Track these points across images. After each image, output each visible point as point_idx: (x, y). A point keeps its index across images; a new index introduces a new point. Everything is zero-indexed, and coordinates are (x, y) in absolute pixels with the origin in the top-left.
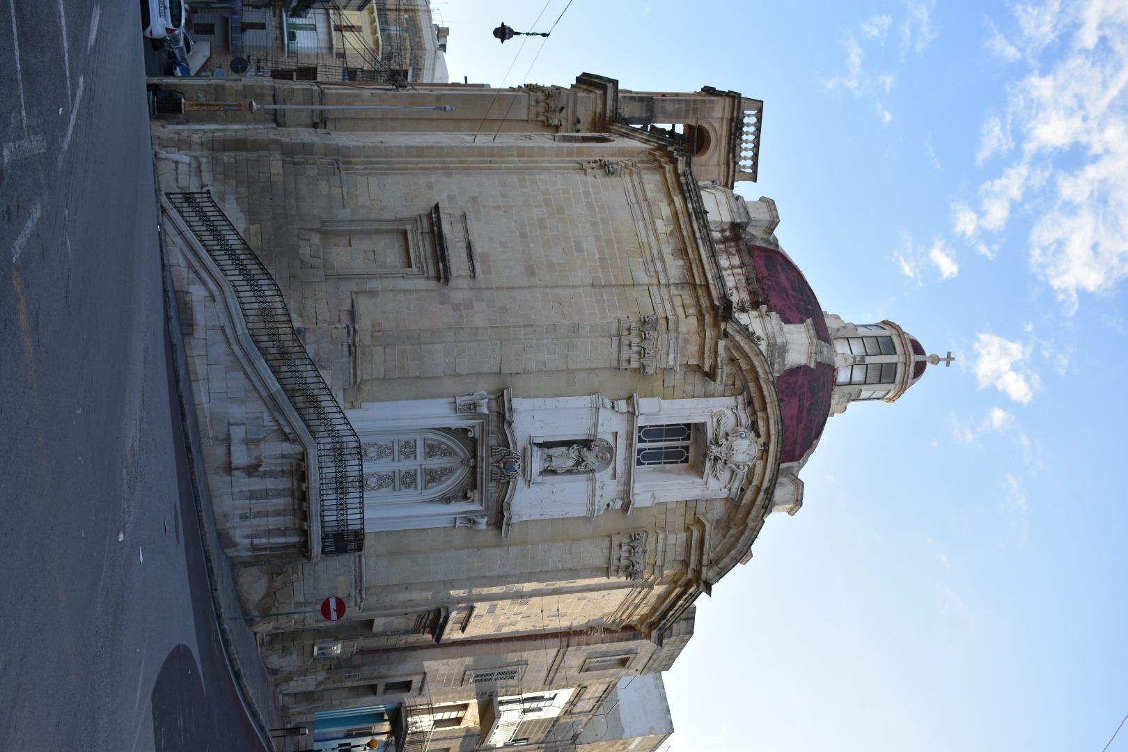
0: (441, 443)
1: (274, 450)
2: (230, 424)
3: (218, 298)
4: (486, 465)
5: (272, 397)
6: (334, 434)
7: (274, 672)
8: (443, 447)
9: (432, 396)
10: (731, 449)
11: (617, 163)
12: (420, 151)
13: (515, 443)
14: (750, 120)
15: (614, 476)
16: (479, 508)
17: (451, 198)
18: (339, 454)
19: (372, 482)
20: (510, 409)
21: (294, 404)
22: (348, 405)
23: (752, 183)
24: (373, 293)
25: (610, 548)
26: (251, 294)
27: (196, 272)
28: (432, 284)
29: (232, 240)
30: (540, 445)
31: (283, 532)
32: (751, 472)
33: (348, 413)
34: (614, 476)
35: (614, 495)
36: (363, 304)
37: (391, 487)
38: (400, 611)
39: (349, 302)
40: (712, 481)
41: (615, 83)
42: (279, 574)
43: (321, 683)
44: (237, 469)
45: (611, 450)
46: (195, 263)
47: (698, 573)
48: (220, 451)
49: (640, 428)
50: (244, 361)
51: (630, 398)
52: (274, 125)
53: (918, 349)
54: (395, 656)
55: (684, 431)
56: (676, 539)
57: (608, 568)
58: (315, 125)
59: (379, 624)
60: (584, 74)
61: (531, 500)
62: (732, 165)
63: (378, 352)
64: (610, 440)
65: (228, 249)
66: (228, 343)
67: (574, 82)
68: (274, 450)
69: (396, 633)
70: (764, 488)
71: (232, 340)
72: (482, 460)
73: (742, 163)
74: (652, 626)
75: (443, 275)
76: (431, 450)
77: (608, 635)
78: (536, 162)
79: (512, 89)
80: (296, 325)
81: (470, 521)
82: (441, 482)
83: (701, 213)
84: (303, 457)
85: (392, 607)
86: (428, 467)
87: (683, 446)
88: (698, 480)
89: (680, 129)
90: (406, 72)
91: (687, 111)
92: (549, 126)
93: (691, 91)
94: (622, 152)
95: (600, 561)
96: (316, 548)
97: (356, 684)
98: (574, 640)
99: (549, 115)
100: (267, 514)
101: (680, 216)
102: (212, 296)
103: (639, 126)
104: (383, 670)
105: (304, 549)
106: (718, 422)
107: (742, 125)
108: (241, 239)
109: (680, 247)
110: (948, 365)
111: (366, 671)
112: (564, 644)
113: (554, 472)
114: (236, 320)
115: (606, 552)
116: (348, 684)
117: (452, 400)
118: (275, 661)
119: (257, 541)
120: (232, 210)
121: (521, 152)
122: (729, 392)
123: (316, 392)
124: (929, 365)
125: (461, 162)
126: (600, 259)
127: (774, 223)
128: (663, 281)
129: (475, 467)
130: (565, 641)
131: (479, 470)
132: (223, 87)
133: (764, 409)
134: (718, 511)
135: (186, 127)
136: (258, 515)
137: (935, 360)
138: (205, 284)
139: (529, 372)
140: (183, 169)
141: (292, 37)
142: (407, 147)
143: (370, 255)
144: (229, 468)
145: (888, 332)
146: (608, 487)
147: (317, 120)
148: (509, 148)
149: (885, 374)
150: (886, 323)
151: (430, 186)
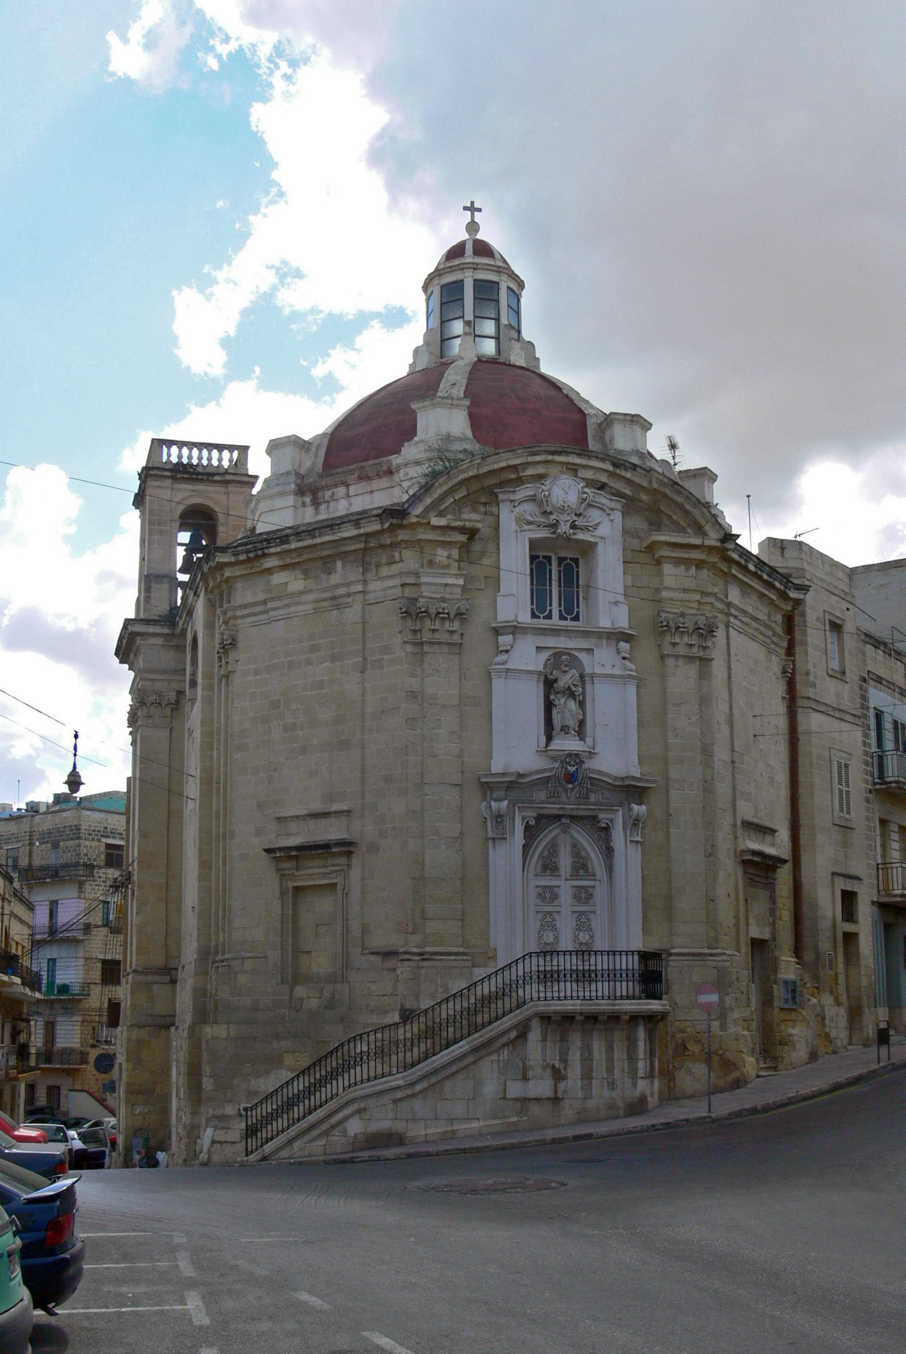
0: (541, 854)
1: (536, 1048)
2: (504, 1098)
3: (362, 1105)
4: (568, 804)
5: (475, 1050)
6: (526, 980)
7: (813, 1056)
8: (545, 853)
9: (486, 865)
10: (562, 509)
11: (222, 634)
12: (205, 865)
13: (544, 770)
14: (173, 455)
15: (590, 651)
16: (620, 813)
17: (258, 833)
18: (546, 977)
19: (584, 937)
20: (503, 774)
21: (484, 1026)
22: (492, 964)
23: (250, 452)
24: (365, 930)
25: (677, 657)
26: (358, 1069)
27: (333, 1127)
28: (356, 861)
29: (300, 1085)
30: (549, 738)
31: (632, 1043)
32: (590, 483)
33: (501, 964)
34: (590, 651)
35: (613, 651)
36: (377, 941)
37: (592, 917)
38: (742, 909)
39: (373, 958)
40: (600, 532)
41: (128, 622)
42: (685, 1048)
43: (838, 1003)
44: (556, 1092)
45: (558, 655)
46: (324, 1127)
47: (711, 549)
48: (535, 1110)
49: (534, 616)
50: (433, 1080)
51: (497, 632)
52: (173, 1029)
53: (456, 252)
54: (805, 909)
55: (539, 565)
56: (672, 575)
57: (701, 659)
58: (173, 982)
59: (756, 932)
60: (117, 654)
61: (614, 754)
62: (228, 477)
63: (431, 927)
64: (545, 655)
65: (309, 1091)
66: (413, 1096)
67: (126, 666)
68: (536, 1048)
69: (772, 912)
70: (611, 468)
71: (409, 1092)
72: (567, 807)
73: (226, 464)
74: (784, 596)
75: (347, 848)
76: (549, 867)
77: (798, 649)
78: (219, 728)
79: (134, 743)
80: (396, 1018)
81: (635, 825)
82: (587, 857)
83: (280, 537)
84: (546, 1018)
85: (737, 917)
86: (569, 871)
87: (560, 567)
88: (600, 549)
89: (184, 537)
90: (108, 846)
91: (162, 532)
92: (177, 702)
93: (138, 522)
94: (210, 625)
95: (692, 670)
96: (654, 1005)
97: (840, 957)
98: (801, 689)
99: (164, 703)
100: (610, 1060)
101: (288, 561)
102: (360, 1111)
103: (180, 593)
104: (825, 924)
105: (652, 1019)
106: (530, 523)
107: (180, 463)
108: (298, 1075)
109: (319, 564)
110: (480, 210)
111: (825, 946)
112: (806, 703)
113: (582, 723)
114: (387, 1086)
115: (681, 662)
116: (841, 967)
117: (490, 843)
118: (800, 1053)
119: (641, 1073)
120: (269, 1083)
121: (207, 747)
122: (495, 509)
123: (472, 1000)
124: (479, 236)
125: (218, 818)
126: (332, 662)
127: (295, 442)
128: (360, 588)
129: (572, 818)
130: (800, 702)
131: (574, 813)
132: (129, 1084)
133: (514, 468)
134: (638, 523)
135: (174, 1130)
136: (610, 1070)
137: (473, 227)
138: (347, 1118)
139: (461, 751)
140: (221, 1136)
141: (64, 989)
142: (199, 880)
143: (321, 930)
144: (556, 1100)
145: (437, 291)
146: (603, 660)
147: (167, 979)
148: (203, 759)
149: (487, 292)
150: (425, 288)
151: (244, 857)
